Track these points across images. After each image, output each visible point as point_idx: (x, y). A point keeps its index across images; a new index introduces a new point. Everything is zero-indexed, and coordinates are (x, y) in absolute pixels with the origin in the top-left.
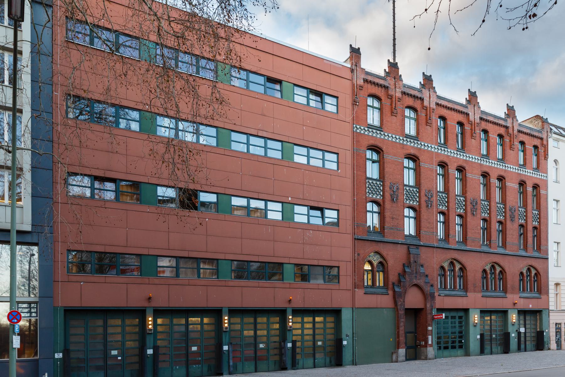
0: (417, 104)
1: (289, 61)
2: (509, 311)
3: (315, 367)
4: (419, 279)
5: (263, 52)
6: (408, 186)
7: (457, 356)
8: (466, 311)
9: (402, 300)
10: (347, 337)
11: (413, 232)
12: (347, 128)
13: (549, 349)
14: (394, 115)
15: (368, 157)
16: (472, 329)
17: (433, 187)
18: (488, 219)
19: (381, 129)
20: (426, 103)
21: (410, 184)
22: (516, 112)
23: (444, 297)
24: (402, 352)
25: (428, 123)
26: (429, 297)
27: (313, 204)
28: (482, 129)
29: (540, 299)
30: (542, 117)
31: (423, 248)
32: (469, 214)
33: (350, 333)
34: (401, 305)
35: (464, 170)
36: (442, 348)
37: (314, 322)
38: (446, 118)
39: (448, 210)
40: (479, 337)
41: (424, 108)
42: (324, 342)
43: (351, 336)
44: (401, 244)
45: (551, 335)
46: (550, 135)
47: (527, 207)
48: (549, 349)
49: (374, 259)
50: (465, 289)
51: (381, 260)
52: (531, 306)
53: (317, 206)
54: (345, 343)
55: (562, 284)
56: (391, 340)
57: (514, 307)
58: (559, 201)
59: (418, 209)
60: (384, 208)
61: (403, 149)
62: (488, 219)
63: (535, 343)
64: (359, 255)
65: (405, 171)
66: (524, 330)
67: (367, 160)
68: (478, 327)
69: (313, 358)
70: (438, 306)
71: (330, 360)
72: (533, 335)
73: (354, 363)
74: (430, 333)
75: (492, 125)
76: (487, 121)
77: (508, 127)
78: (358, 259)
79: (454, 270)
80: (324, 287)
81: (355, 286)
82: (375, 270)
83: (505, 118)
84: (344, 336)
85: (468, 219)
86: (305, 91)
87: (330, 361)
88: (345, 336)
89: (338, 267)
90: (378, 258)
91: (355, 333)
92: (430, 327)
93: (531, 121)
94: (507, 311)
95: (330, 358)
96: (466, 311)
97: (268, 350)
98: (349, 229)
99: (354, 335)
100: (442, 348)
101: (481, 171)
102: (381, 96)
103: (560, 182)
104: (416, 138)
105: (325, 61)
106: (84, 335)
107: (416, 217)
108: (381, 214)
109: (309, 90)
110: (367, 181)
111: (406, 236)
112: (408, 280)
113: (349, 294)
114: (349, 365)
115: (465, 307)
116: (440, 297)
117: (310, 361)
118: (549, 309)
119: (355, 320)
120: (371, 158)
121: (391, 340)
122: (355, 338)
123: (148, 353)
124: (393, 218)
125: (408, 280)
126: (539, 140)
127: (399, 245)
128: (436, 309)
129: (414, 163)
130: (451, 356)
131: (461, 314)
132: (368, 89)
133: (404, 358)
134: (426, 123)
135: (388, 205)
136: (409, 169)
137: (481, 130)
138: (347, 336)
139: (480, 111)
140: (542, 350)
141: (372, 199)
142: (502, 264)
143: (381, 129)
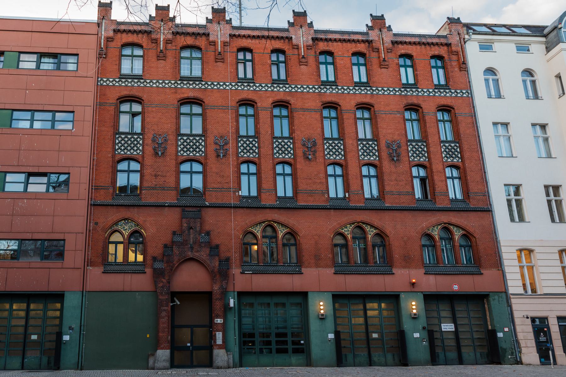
0: (201, 42)
1: (15, 32)
2: (402, 296)
3: (22, 368)
4: (197, 251)
5: (55, 34)
6: (447, 142)
7: (290, 365)
8: (304, 295)
9: (164, 281)
10: (70, 329)
11: (459, 196)
12: (90, 85)
13: (519, 362)
14: (383, 68)
15: (406, 117)
16: (314, 325)
17: (229, 132)
18: (461, 165)
19: (416, 87)
20: (294, 41)
21: (449, 139)
22: (386, 21)
23: (253, 275)
24: (163, 354)
25: (462, 68)
26: (218, 276)
27: (31, 170)
28: (319, 51)
29: (481, 275)
30: (453, 22)
31: (209, 209)
32: (300, 159)
33: (75, 325)
34: (162, 287)
35: (288, 105)
36: (274, 351)
37: (28, 310)
38: (333, 51)
39: (346, 160)
40: (331, 336)
41: (374, 50)
42: (381, 334)
43: (77, 328)
44: (168, 206)
45: (520, 336)
46: (467, 37)
47: (427, 139)
48: (519, 362)
49: (124, 228)
50: (300, 263)
51: (464, 232)
52: (456, 287)
53: (37, 171)
54: (66, 338)
55: (537, 250)
56: (148, 336)
57: (413, 290)
58: (509, 123)
59: (428, 165)
60: (431, 170)
61: (176, 93)
62: (461, 165)
63: (485, 351)
64: (96, 224)
65: (440, 125)
66: (453, 327)
67: (357, 120)
68: (330, 323)
69: (21, 356)
70: (239, 288)
71: (48, 360)
72: (476, 336)
73: (80, 367)
74: (220, 328)
75: (339, 44)
76: (401, 43)
77: (372, 41)
78: (94, 229)
79: (451, 239)
80: (39, 265)
81: (89, 263)
82: (349, 244)
83: (367, 31)
84: (65, 329)
85: (298, 166)
86: (35, 56)
87: (49, 363)
88: (68, 329)
89: (64, 240)
90: (132, 226)
91: (84, 326)
92: (219, 320)
93: (445, 27)
94: (399, 295)
95: (49, 358)
96: (304, 295)
97: (383, 340)
98: (84, 193)
99: (82, 328)
100: (274, 351)
101: (322, 102)
102: (141, 42)
103: (505, 97)
104: (446, 86)
105: (61, 23)
106: (468, 318)
107: (460, 177)
108: (380, 178)
109: (39, 54)
110: (442, 145)
111: (367, 199)
112: (178, 253)
113: (78, 274)
114: (71, 369)
115: (305, 290)
116: (244, 275)
117: (17, 361)
118: (506, 292)
119: (85, 308)
120: (442, 119)
121: (148, 336)
122: (84, 332)
123: (64, 339)
124: (156, 176)
125: (178, 253)
126: (446, 48)
127: (167, 209)
128: (236, 293)
129: (416, 113)
130: (273, 365)
131: (299, 300)
132: (121, 39)
133: (167, 364)
134: (460, 69)
135: (387, 166)
136: (443, 122)
137: (318, 53)
138: (70, 328)
139: (312, 31)
140: (500, 363)
141: (331, 161)
142: (376, 223)
143: (416, 87)
